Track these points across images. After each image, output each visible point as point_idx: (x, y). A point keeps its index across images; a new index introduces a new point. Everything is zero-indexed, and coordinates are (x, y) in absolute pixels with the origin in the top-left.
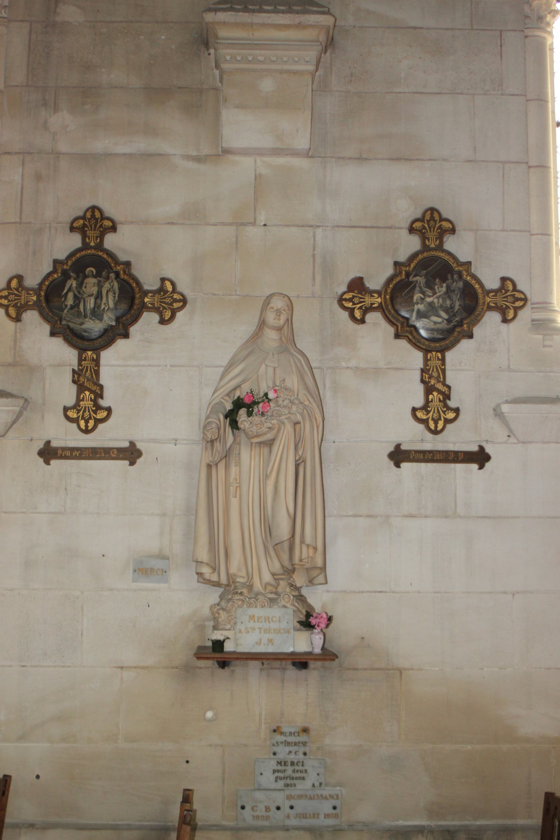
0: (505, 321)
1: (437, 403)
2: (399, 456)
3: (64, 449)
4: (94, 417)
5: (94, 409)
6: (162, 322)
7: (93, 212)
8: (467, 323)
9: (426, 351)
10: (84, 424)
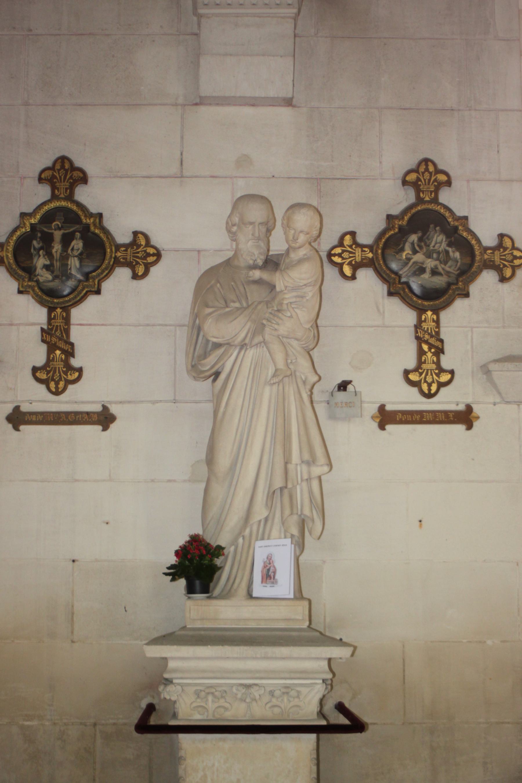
0: (503, 279)
1: (429, 364)
2: (17, 418)
3: (31, 414)
4: (64, 378)
5: (65, 369)
6: (135, 277)
7: (63, 163)
8: (462, 281)
9: (421, 311)
10: (54, 386)
